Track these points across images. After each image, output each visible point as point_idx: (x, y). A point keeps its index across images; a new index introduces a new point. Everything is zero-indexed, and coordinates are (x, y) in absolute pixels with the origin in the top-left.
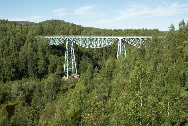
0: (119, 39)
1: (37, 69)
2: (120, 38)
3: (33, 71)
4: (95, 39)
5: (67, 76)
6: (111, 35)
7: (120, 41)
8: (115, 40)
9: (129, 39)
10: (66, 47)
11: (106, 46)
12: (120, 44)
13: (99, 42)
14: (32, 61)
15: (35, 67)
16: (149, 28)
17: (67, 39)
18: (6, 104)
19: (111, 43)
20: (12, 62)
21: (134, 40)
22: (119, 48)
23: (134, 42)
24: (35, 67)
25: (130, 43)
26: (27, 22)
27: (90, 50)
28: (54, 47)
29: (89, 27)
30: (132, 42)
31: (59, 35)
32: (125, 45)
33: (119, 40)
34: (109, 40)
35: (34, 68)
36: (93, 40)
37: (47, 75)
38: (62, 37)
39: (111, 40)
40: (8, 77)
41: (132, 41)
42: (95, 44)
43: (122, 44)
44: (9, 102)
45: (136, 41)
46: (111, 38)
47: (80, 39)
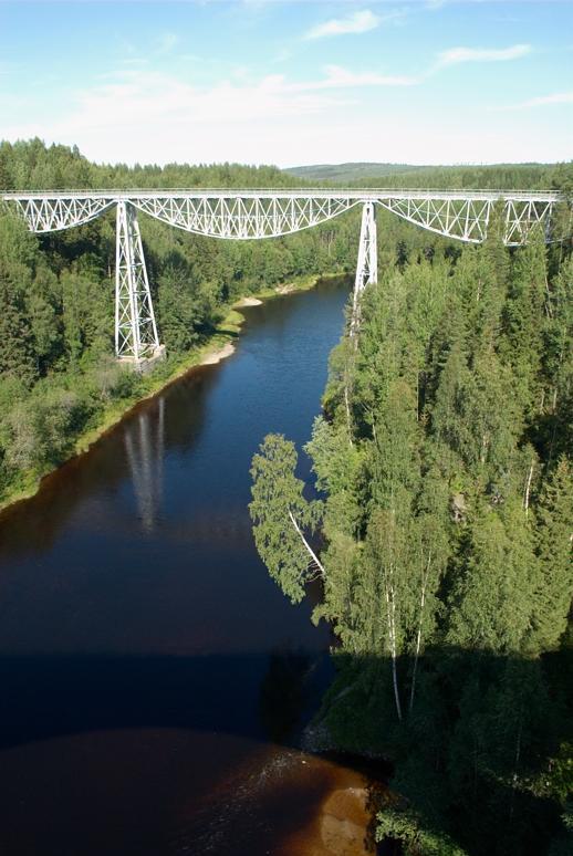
0: (115, 204)
1: (32, 339)
2: (122, 198)
3: (19, 345)
9: (152, 201)
12: (121, 216)
14: (8, 303)
15: (25, 331)
16: (193, 162)
19: (90, 215)
23: (168, 213)
26: (437, 169)
27: (535, 186)
30: (162, 212)
31: (39, 187)
32: (136, 224)
34: (84, 207)
35: (22, 333)
36: (39, 206)
38: (94, 198)
39: (90, 206)
41: (162, 208)
42: (293, 206)
44: (8, 490)
45: (174, 207)
47: (45, 202)
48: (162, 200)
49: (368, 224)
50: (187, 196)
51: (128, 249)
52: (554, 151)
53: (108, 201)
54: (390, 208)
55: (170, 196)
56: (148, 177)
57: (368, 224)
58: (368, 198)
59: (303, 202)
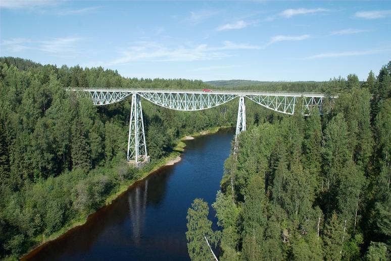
2: (134, 92)
3: (84, 154)
4: (171, 96)
5: (134, 159)
6: (303, 91)
7: (242, 100)
8: (127, 95)
10: (132, 108)
11: (112, 102)
12: (134, 100)
13: (103, 97)
14: (81, 135)
15: (87, 148)
16: (166, 78)
17: (132, 94)
18: (69, 225)
20: (47, 141)
21: (155, 96)
22: (134, 106)
23: (155, 99)
24: (86, 147)
25: (149, 100)
28: (102, 110)
29: (238, 80)
30: (152, 98)
33: (133, 96)
34: (118, 95)
35: (86, 148)
37: (103, 160)
38: (122, 92)
40: (35, 170)
41: (152, 97)
43: (137, 101)
44: (72, 221)
46: (226, 95)
48: (152, 94)
49: (242, 106)
50: (163, 92)
51: (136, 114)
52: (365, 61)
53: (128, 93)
54: (251, 99)
55: (156, 92)
56: (147, 84)
57: (242, 106)
58: (242, 95)
59: (213, 95)
